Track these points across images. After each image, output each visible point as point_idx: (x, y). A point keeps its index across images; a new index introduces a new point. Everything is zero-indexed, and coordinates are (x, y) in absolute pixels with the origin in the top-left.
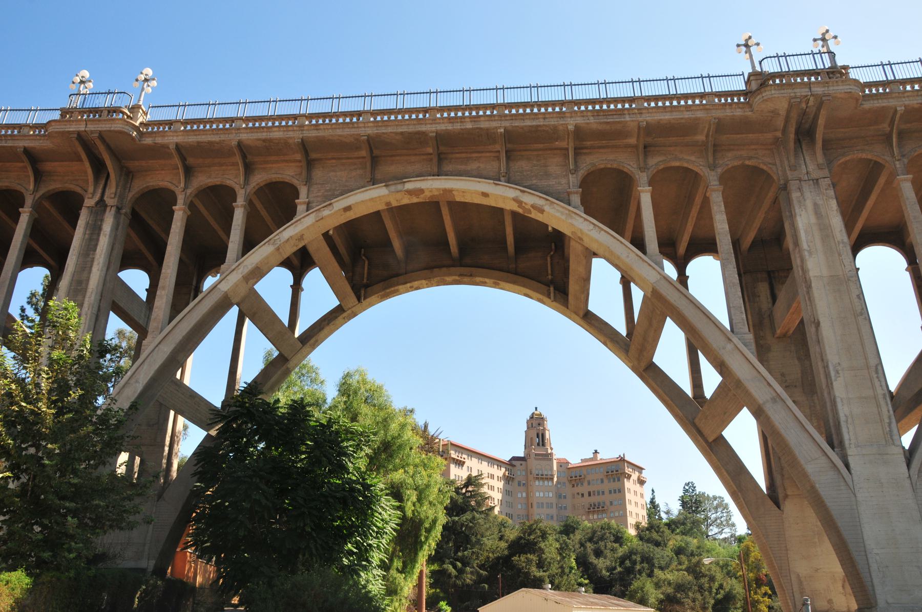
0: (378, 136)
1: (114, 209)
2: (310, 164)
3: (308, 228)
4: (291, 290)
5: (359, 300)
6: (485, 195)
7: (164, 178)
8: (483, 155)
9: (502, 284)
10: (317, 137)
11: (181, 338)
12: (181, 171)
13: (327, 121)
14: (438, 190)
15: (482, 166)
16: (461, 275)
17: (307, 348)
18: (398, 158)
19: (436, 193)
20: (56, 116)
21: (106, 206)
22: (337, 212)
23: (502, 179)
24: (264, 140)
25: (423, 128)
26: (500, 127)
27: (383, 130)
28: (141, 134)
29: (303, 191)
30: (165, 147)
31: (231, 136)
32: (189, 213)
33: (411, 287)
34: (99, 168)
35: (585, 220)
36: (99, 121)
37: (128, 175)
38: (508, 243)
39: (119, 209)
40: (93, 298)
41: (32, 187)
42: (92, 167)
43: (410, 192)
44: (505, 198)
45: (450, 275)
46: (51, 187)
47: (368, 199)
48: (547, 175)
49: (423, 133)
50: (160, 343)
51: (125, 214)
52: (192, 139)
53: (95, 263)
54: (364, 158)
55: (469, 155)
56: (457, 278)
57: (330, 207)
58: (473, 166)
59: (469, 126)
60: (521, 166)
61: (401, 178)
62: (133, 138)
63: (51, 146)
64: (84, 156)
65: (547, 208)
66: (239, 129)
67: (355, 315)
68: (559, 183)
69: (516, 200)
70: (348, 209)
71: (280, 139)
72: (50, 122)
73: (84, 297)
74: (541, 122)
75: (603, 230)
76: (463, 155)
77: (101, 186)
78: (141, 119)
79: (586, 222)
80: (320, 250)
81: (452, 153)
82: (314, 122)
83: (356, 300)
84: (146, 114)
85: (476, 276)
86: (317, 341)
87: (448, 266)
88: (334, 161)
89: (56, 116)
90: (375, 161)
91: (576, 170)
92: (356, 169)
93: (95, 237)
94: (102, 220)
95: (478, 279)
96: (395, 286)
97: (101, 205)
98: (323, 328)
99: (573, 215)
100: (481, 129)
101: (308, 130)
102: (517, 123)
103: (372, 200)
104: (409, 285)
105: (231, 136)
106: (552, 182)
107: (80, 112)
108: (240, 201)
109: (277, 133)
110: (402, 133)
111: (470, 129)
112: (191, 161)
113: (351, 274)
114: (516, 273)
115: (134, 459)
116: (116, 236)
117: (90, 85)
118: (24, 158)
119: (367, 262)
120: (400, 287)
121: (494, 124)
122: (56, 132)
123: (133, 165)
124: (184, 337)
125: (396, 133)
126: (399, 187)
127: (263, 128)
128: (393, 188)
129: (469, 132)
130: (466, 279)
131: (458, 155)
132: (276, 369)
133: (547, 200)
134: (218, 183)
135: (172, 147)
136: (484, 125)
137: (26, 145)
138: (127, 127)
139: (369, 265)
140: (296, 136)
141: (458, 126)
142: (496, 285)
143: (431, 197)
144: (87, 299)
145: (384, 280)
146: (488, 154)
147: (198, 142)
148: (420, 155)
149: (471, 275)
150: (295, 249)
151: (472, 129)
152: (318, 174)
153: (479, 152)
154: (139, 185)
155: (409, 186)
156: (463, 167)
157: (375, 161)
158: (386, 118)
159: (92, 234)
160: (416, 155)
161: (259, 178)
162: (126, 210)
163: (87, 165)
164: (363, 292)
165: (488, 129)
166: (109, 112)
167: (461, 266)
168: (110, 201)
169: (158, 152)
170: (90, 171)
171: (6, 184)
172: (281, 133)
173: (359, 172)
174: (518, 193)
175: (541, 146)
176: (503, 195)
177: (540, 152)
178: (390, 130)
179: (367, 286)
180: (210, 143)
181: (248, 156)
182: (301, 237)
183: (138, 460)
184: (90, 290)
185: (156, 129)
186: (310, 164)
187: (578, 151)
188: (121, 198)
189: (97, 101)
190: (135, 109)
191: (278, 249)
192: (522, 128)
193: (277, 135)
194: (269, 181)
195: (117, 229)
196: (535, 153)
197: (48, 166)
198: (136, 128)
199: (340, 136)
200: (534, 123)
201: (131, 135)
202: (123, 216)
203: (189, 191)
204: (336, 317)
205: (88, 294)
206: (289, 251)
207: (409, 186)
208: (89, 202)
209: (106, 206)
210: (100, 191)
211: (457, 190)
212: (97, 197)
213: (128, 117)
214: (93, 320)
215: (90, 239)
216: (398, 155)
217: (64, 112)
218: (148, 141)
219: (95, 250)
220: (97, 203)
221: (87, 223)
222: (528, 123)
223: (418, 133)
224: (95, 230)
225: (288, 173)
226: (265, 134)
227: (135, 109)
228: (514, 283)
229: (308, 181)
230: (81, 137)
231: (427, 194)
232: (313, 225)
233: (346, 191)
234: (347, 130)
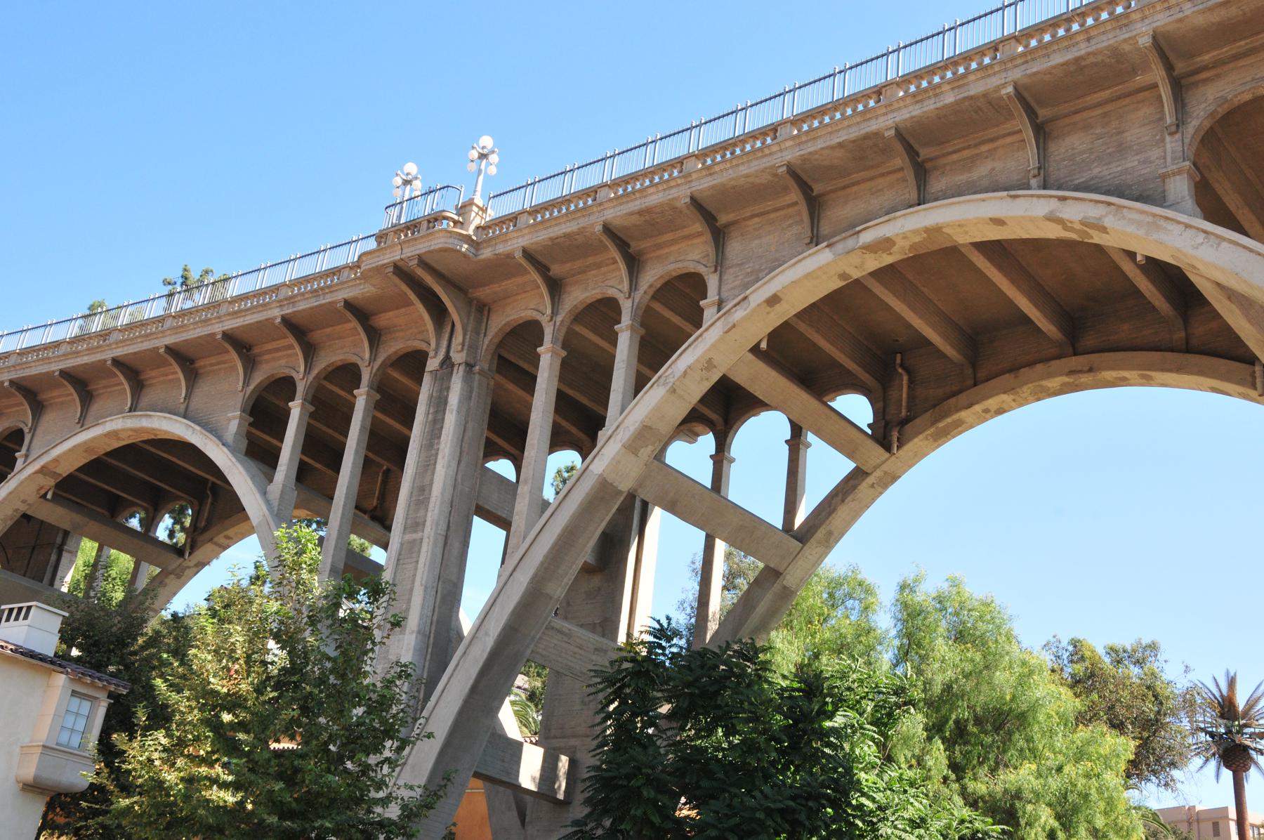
0: (804, 160)
1: (462, 368)
2: (719, 235)
3: (714, 346)
4: (787, 447)
5: (888, 448)
6: (998, 222)
7: (531, 303)
8: (1000, 142)
9: (1157, 375)
10: (712, 187)
11: (541, 558)
12: (544, 290)
13: (738, 151)
14: (916, 232)
15: (998, 165)
16: (1071, 373)
17: (811, 549)
18: (855, 188)
19: (917, 239)
20: (372, 244)
21: (453, 365)
22: (754, 310)
23: (1033, 182)
24: (640, 213)
25: (873, 126)
26: (1003, 83)
27: (810, 148)
28: (476, 245)
29: (712, 282)
30: (509, 256)
31: (593, 218)
32: (564, 353)
33: (986, 411)
34: (438, 312)
35: (1187, 226)
36: (416, 239)
37: (481, 310)
38: (1147, 294)
39: (469, 366)
40: (436, 511)
41: (367, 356)
42: (429, 310)
43: (870, 248)
44: (1033, 220)
45: (1050, 375)
46: (391, 351)
47: (806, 275)
48: (1122, 150)
49: (877, 135)
50: (514, 570)
51: (481, 373)
52: (543, 236)
53: (440, 457)
54: (796, 204)
55: (976, 151)
56: (1066, 379)
57: (744, 304)
58: (981, 171)
59: (949, 98)
60: (1071, 146)
61: (852, 227)
62: (464, 255)
63: (373, 290)
64: (413, 297)
65: (1108, 222)
66: (1012, 59)
67: (895, 478)
68: (1146, 161)
69: (1051, 218)
70: (773, 300)
71: (662, 205)
72: (360, 257)
73: (427, 510)
74: (1082, 49)
75: (1224, 239)
76: (966, 153)
77: (447, 336)
78: (476, 220)
79: (1190, 232)
80: (759, 377)
81: (944, 155)
82: (913, 88)
83: (881, 451)
84: (484, 210)
85: (1100, 369)
86: (830, 533)
87: (1046, 360)
88: (757, 220)
89: (372, 244)
90: (815, 205)
91: (1180, 123)
92: (790, 226)
93: (440, 417)
94: (448, 388)
95: (1109, 375)
96: (958, 410)
97: (447, 362)
98: (835, 510)
99: (1162, 222)
100: (971, 98)
101: (698, 179)
102: (1035, 68)
103: (808, 276)
104: (977, 408)
105: (593, 218)
106: (1132, 162)
107: (395, 232)
108: (626, 319)
109: (655, 197)
110: (840, 145)
111: (952, 104)
112: (556, 270)
113: (881, 404)
114: (1188, 349)
115: (557, 759)
116: (469, 409)
117: (417, 184)
118: (349, 315)
119: (905, 378)
120: (963, 414)
121: (994, 82)
122: (370, 270)
123: (483, 293)
124: (546, 557)
125: (832, 148)
126: (851, 243)
127: (926, 90)
128: (840, 248)
129: (955, 108)
130: (1084, 379)
131: (955, 157)
132: (768, 594)
133: (1109, 204)
134: (599, 297)
135: (518, 255)
136: (976, 88)
137: (346, 296)
138: (451, 240)
139: (911, 381)
140: (681, 195)
141: (930, 106)
142: (1147, 381)
143: (912, 247)
144: (429, 514)
145: (934, 406)
146: (1009, 140)
147: (551, 239)
148: (889, 173)
149: (1090, 370)
150: (707, 386)
151: (957, 103)
152: (734, 248)
153: (992, 140)
154: (500, 321)
155: (867, 237)
156: (962, 178)
157: (815, 205)
158: (816, 124)
159: (436, 412)
160: (882, 175)
161: (652, 276)
162: (483, 364)
163: (420, 307)
164: (895, 435)
165: (985, 95)
166: (429, 222)
167: (1075, 353)
168: (458, 357)
169: (502, 267)
170: (426, 316)
171: (341, 357)
172: (661, 195)
173: (796, 229)
174: (1054, 204)
175: (1106, 94)
176: (1030, 215)
177: (1108, 108)
178: (820, 144)
179: (907, 420)
180: (567, 236)
181: (627, 245)
182: (709, 365)
183: (564, 761)
184: (433, 500)
185: (556, 213)
186: (719, 235)
187: (1180, 87)
188: (473, 348)
189: (415, 210)
190: (464, 209)
191: (673, 391)
192: (1049, 72)
193: (655, 199)
194: (667, 278)
195: (470, 398)
196: (1099, 111)
197: (382, 320)
198: (467, 239)
199: (747, 176)
200: (1069, 56)
201: (459, 251)
202: (477, 376)
203: (559, 319)
204: (855, 487)
205: (431, 506)
206: (697, 390)
207: (867, 237)
208: (432, 364)
209: (453, 365)
210: (444, 343)
211: (948, 225)
212: (441, 356)
213: (455, 222)
214: (441, 544)
215: (435, 421)
216: (853, 184)
217: (381, 237)
218: (486, 253)
219: (439, 437)
220: (442, 364)
221: (431, 397)
222: (1058, 59)
223: (867, 137)
224: (440, 403)
225: (691, 254)
226: (637, 202)
227: (464, 209)
228: (1179, 369)
229: (719, 264)
230: (400, 270)
231: (901, 243)
232: (721, 340)
233: (775, 264)
234: (756, 163)
